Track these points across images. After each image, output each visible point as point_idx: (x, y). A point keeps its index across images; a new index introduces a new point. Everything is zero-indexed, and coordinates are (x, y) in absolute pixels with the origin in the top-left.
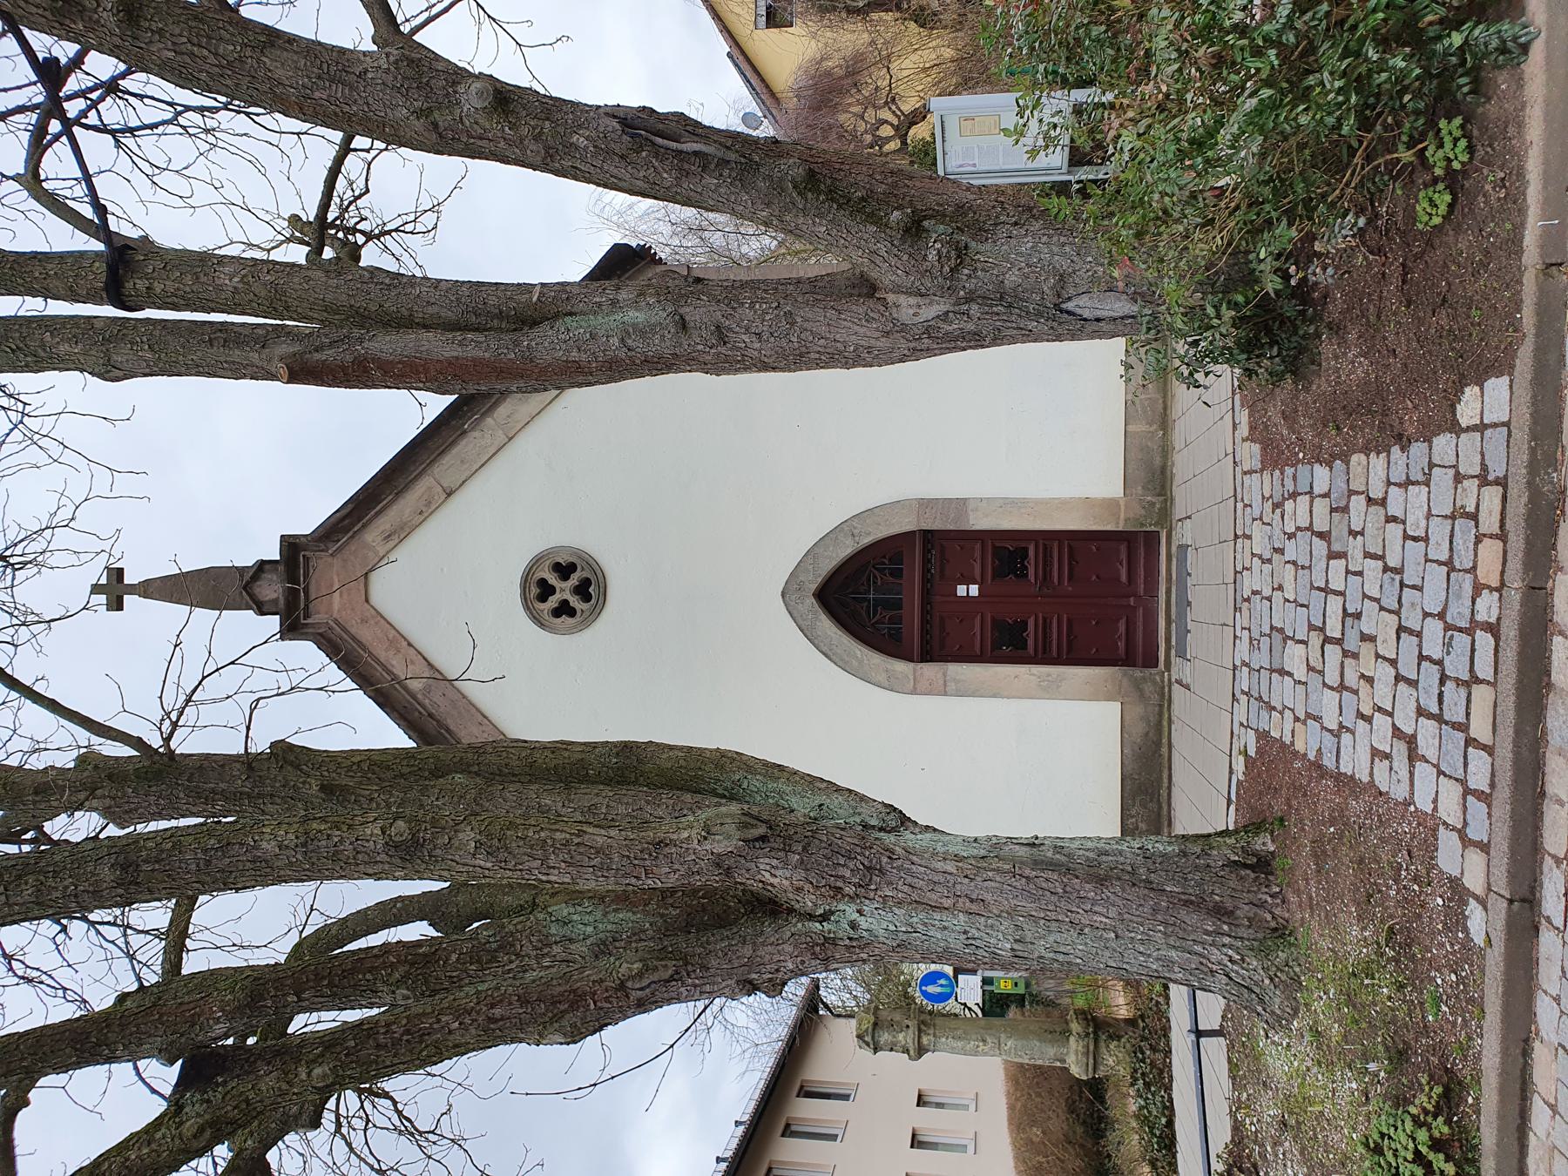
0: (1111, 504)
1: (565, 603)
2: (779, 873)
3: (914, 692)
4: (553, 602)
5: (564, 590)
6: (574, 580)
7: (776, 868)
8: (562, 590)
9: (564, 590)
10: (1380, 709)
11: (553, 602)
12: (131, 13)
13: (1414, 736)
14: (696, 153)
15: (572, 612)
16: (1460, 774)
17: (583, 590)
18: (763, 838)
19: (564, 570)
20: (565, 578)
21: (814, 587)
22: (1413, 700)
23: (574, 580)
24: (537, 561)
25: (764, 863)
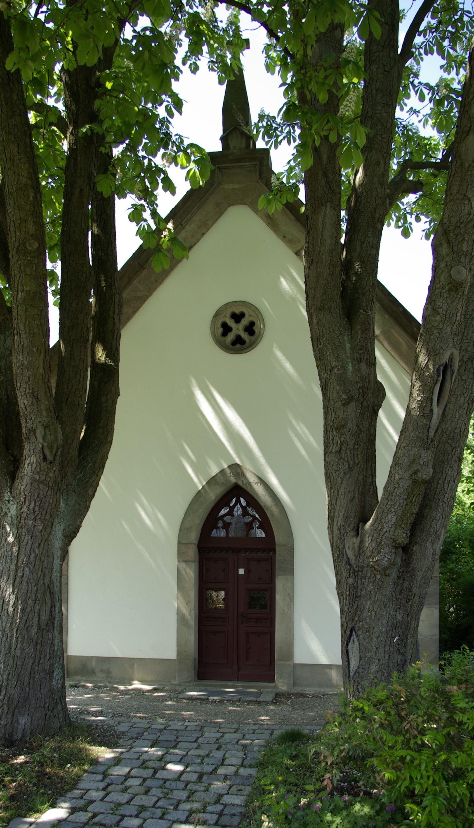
0: (290, 654)
1: (230, 329)
2: (30, 467)
3: (179, 543)
4: (231, 323)
5: (238, 329)
6: (245, 336)
7: (32, 465)
8: (238, 329)
9: (238, 329)
10: (107, 795)
11: (231, 323)
12: (47, 2)
13: (86, 811)
14: (431, 410)
15: (225, 334)
16: (171, 822)
17: (239, 341)
18: (45, 458)
19: (250, 329)
20: (230, 329)
21: (240, 483)
22: (101, 811)
23: (245, 336)
24: (256, 310)
25: (33, 459)
